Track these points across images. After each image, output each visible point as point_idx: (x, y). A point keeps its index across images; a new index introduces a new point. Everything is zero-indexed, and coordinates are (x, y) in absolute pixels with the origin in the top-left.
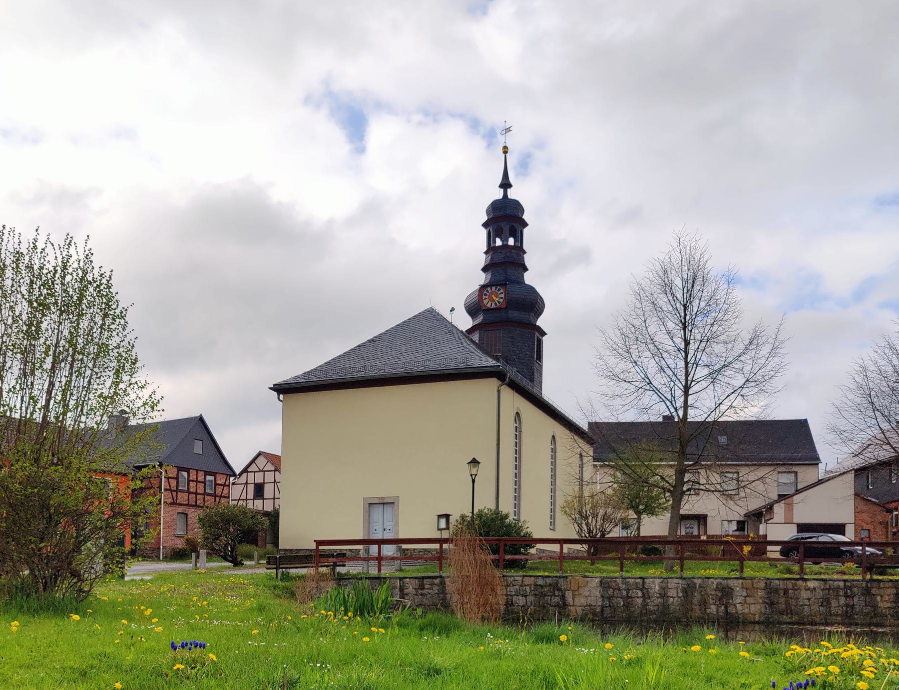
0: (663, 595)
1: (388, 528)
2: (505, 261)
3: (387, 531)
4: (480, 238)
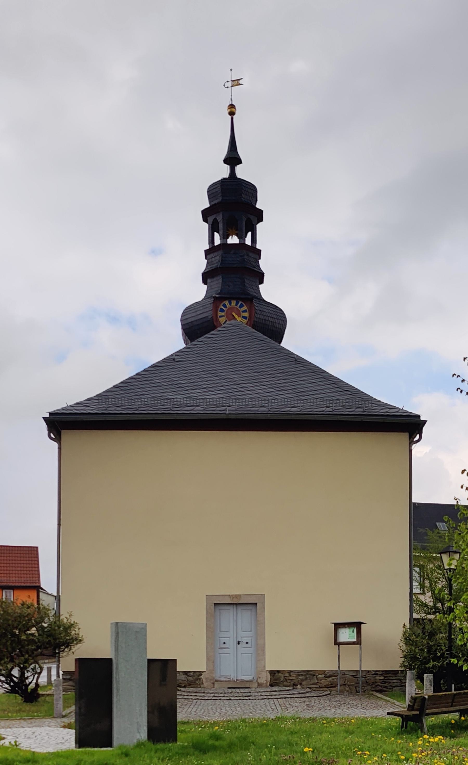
1: (245, 640)
2: (234, 271)
3: (243, 645)
4: (199, 237)
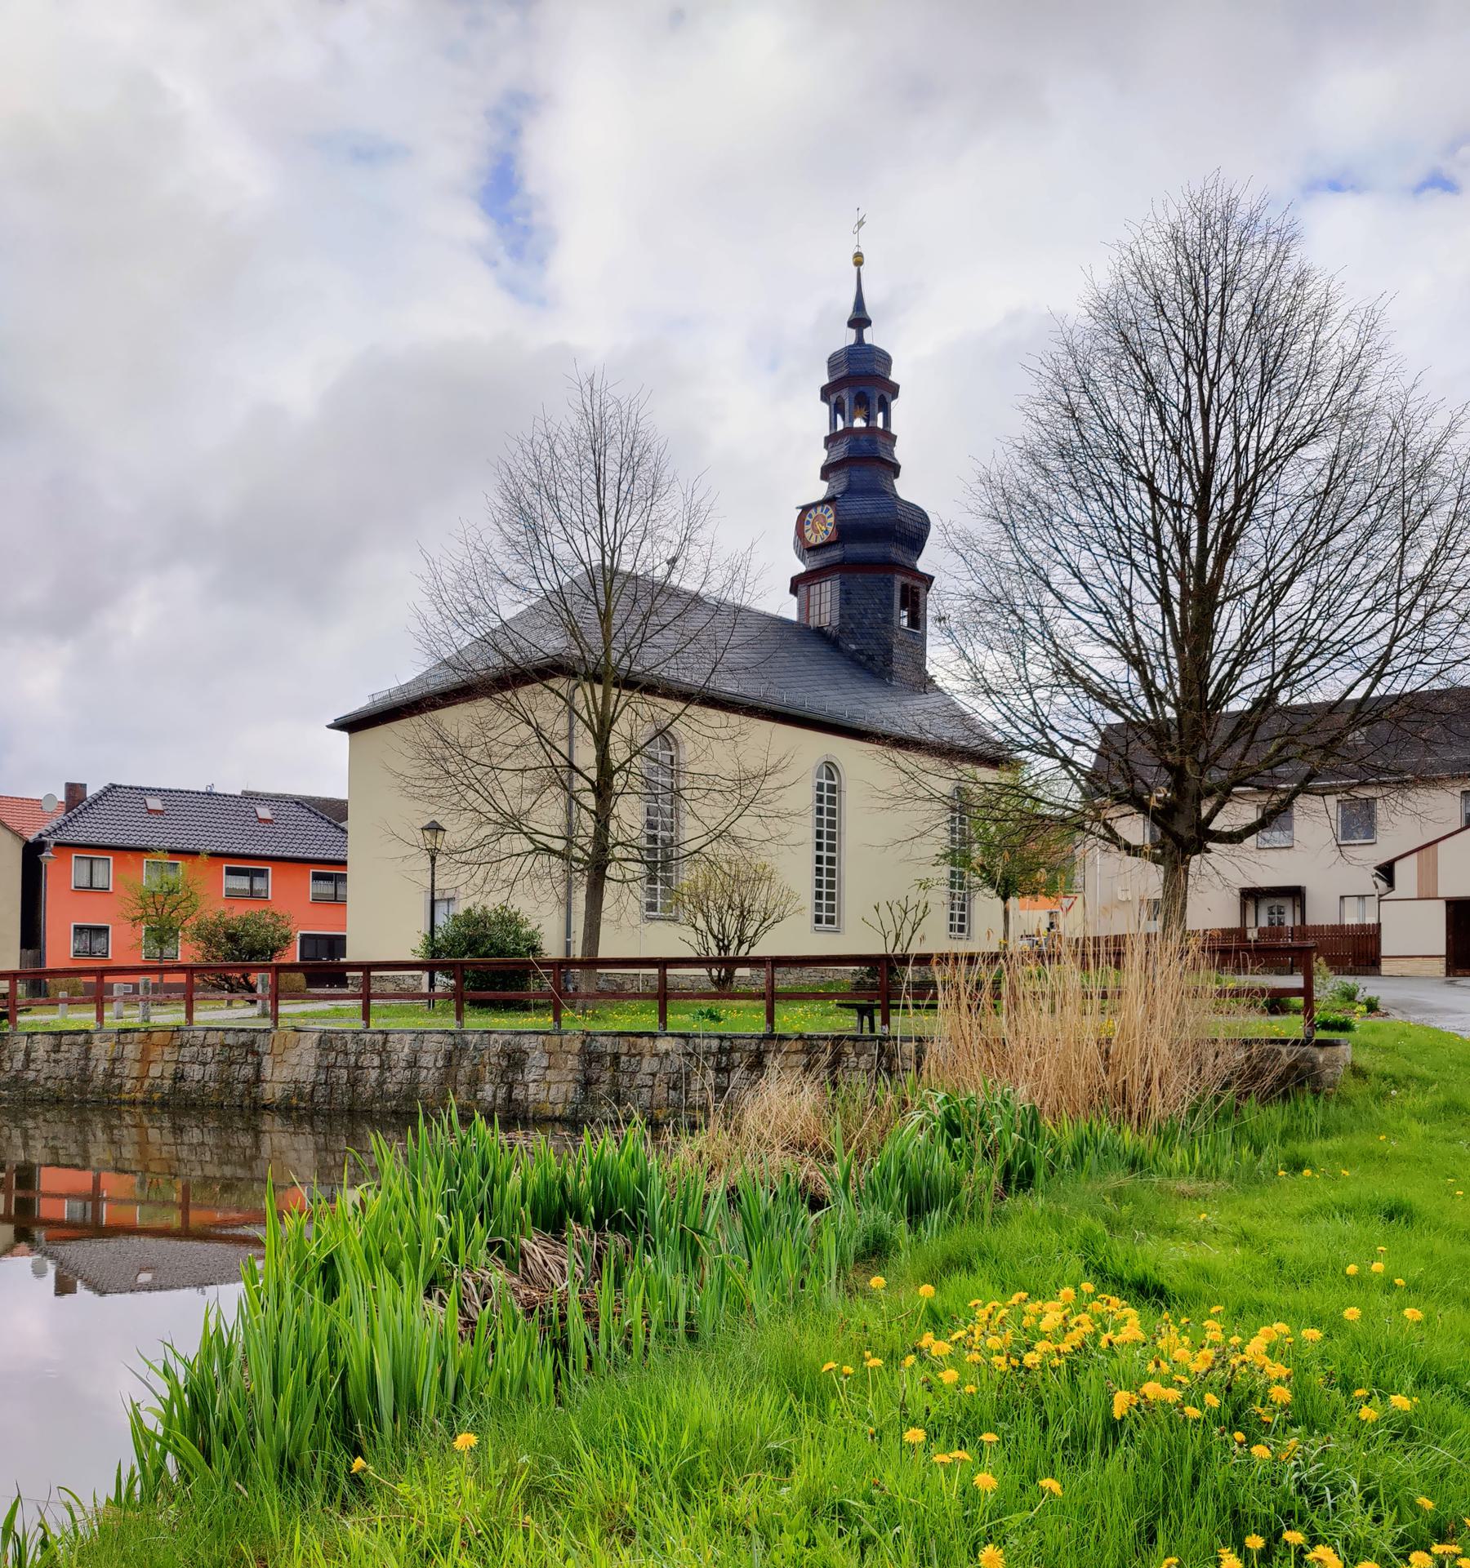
0: (413, 1064)
2: (862, 461)
4: (817, 419)
